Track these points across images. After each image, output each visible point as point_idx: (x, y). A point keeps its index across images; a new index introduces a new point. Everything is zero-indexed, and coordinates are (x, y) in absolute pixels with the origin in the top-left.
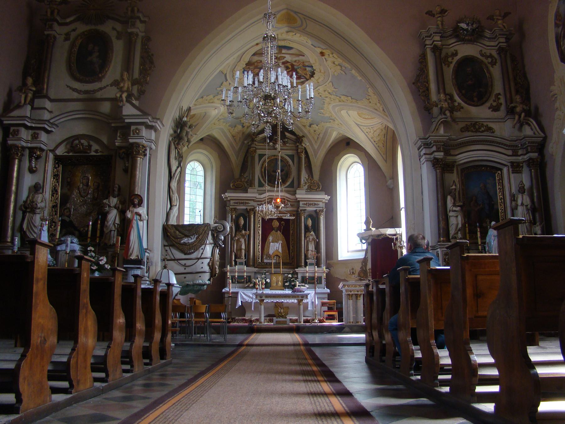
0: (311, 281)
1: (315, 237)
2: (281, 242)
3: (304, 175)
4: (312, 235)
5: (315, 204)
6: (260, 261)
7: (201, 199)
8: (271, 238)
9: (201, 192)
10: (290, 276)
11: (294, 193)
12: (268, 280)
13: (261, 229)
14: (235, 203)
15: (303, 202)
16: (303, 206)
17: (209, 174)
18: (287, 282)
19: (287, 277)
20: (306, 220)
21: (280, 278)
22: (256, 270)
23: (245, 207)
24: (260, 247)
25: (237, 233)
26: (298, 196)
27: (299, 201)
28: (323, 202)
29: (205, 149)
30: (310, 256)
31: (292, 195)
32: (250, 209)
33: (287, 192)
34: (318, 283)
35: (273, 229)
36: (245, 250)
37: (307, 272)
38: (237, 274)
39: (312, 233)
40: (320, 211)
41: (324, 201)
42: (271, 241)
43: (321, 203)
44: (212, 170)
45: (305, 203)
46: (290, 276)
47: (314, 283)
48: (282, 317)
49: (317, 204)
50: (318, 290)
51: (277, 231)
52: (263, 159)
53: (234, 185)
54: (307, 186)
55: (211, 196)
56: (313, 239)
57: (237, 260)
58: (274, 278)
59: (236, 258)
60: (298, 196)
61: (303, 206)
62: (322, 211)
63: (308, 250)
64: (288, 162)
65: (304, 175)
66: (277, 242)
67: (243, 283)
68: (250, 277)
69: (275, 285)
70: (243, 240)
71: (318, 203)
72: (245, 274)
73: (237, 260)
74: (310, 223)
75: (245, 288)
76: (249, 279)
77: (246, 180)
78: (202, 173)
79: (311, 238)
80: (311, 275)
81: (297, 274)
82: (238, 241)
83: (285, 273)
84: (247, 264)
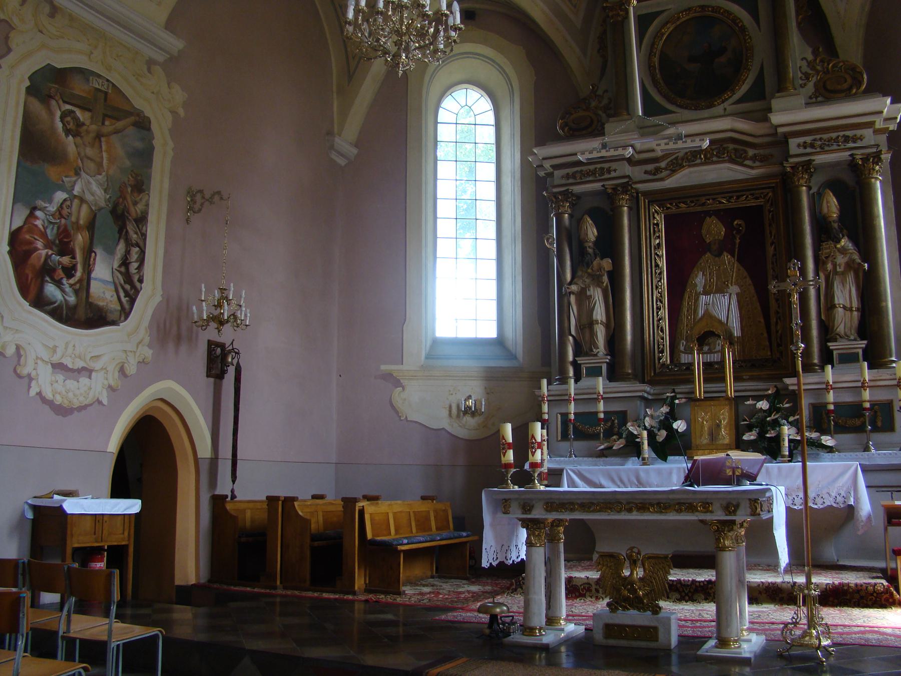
0: (850, 422)
1: (856, 257)
2: (734, 289)
3: (799, 52)
4: (843, 251)
5: (847, 139)
6: (666, 358)
7: (490, 191)
8: (699, 280)
9: (488, 171)
10: (763, 405)
11: (763, 116)
12: (680, 425)
13: (663, 252)
14: (568, 176)
15: (801, 140)
16: (801, 151)
17: (506, 113)
18: (750, 428)
19: (754, 411)
20: (816, 200)
21: (725, 416)
22: (645, 389)
23: (597, 186)
24: (665, 313)
25: (580, 273)
26: (776, 118)
27: (786, 137)
28: (877, 132)
29: (485, 42)
30: (841, 329)
31: (757, 121)
32: (615, 189)
33: (744, 115)
34: (876, 429)
35: (703, 248)
36: (607, 326)
37: (827, 387)
38: (572, 408)
39: (844, 242)
40: (866, 159)
41: (879, 124)
42: (700, 289)
43: (867, 133)
44: (512, 101)
45: (808, 139)
46: (763, 405)
47: (860, 429)
48: (637, 603)
49: (855, 139)
50: (878, 456)
51: (719, 255)
52: (651, 29)
53: (566, 124)
54: (811, 85)
55: (513, 177)
56: (850, 265)
57: (580, 360)
58: (704, 418)
59: (578, 352)
60: (776, 118)
61: (801, 151)
62: (877, 157)
63: (831, 306)
64: (736, 20)
65: (799, 52)
66: (721, 290)
67: (595, 437)
68: (623, 417)
69: (705, 440)
70: (597, 295)
71: (859, 132)
72: (601, 406)
73: (580, 360)
74: (832, 206)
75: (602, 454)
76: (616, 423)
77: (605, 101)
78: (490, 118)
79: (841, 260)
80: (848, 398)
81: (794, 397)
82: (583, 297)
83: (747, 398)
84: (614, 374)
